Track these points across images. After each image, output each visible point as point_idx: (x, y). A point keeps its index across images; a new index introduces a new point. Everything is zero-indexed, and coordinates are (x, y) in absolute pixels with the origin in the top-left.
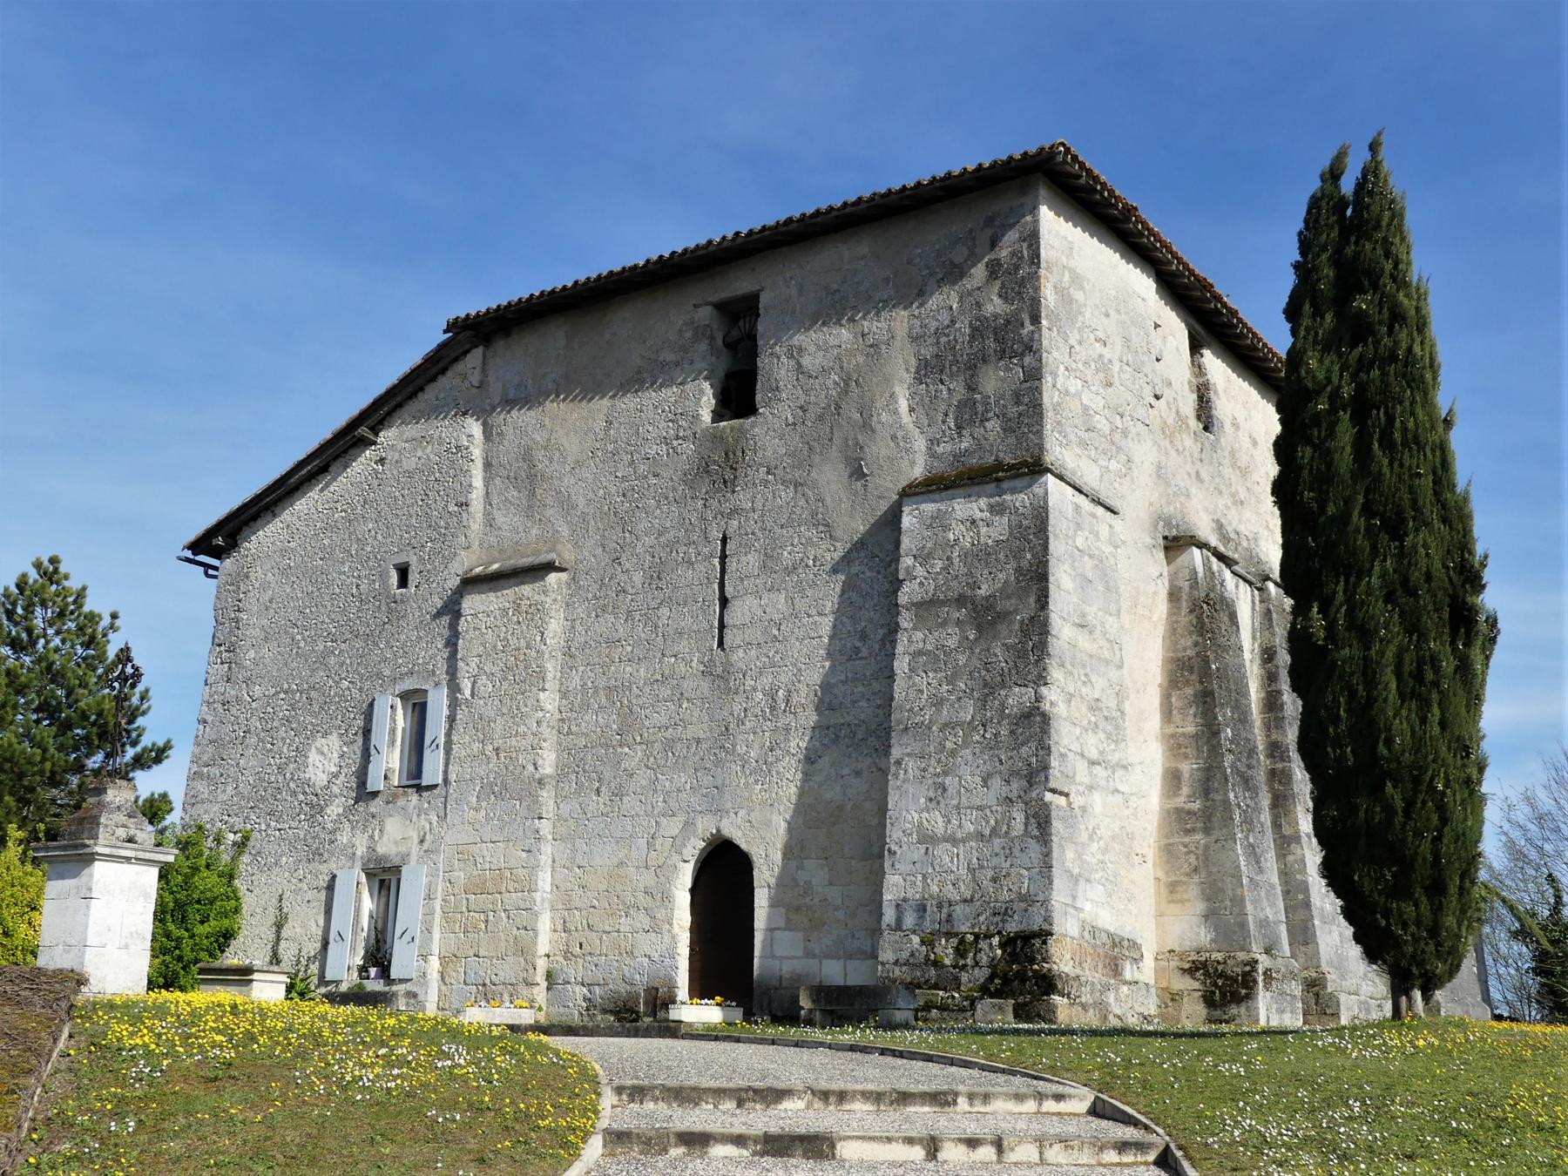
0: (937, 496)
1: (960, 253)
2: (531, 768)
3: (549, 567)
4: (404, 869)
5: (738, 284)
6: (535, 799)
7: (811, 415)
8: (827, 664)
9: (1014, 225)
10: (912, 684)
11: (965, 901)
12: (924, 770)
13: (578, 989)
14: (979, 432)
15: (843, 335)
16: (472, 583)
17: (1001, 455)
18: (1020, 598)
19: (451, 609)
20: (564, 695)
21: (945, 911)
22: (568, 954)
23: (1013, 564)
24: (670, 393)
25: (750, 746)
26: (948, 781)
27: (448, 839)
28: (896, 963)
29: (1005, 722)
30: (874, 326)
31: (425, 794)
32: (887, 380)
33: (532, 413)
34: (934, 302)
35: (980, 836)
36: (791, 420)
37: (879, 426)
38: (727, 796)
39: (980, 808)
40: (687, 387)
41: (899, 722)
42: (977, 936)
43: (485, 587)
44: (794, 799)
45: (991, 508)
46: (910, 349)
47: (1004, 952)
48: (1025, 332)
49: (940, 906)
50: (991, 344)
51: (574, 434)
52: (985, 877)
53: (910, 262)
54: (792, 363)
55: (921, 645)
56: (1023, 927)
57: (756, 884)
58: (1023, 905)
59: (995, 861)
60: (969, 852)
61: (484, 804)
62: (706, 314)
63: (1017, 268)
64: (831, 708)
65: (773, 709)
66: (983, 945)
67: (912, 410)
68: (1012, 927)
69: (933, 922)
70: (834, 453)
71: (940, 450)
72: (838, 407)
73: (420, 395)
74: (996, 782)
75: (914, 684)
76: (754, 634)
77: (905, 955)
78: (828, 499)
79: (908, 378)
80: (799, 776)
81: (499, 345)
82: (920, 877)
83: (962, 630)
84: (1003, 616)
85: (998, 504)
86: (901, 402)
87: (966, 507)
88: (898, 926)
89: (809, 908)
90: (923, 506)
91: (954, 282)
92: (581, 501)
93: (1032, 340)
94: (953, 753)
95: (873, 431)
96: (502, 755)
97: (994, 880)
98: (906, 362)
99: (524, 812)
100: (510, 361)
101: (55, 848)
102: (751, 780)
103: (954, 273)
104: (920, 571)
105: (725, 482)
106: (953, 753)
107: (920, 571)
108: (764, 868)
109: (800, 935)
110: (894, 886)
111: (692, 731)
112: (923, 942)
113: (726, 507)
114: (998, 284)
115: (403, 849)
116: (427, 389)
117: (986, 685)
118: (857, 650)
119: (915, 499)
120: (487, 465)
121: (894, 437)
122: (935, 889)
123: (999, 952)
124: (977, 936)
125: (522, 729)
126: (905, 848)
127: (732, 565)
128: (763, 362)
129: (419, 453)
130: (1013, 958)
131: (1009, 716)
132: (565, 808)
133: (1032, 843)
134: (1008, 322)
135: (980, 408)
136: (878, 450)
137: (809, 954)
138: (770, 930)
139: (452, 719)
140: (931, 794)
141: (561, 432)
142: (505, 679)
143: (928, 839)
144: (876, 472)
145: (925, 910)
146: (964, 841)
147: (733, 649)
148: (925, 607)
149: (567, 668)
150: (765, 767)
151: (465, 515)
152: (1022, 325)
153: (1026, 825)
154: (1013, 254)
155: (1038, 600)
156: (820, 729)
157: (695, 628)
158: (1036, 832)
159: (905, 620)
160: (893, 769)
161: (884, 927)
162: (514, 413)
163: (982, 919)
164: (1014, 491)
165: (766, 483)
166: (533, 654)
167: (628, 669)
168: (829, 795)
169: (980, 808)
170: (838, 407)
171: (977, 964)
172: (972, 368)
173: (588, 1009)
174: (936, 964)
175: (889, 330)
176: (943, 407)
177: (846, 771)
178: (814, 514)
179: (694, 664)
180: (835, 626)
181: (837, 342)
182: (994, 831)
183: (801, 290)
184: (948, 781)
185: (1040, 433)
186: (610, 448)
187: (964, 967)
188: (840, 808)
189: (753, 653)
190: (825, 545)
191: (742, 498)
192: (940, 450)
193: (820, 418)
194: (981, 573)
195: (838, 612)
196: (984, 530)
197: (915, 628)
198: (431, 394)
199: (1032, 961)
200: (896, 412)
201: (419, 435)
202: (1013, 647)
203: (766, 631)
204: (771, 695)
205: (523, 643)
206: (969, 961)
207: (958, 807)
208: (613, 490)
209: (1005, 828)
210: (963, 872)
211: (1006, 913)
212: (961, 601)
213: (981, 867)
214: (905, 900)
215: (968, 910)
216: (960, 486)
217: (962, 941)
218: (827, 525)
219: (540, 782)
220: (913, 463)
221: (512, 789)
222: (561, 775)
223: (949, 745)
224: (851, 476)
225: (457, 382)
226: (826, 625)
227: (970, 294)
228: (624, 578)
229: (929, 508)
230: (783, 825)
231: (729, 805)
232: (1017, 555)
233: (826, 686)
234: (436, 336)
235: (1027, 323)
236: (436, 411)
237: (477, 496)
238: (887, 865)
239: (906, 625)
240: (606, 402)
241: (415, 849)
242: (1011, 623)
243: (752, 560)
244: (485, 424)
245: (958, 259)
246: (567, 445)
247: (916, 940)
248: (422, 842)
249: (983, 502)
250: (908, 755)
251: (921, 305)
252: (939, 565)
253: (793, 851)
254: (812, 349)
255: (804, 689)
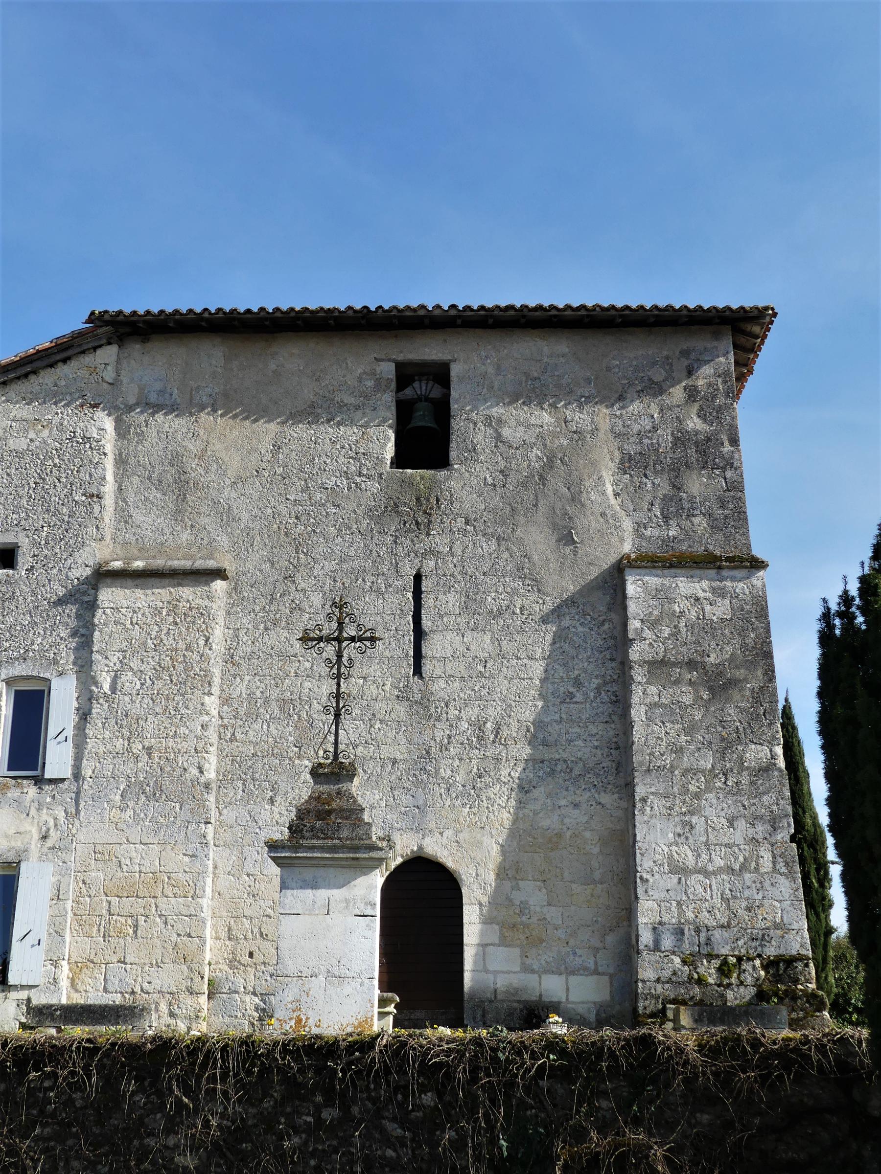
0: (659, 572)
1: (658, 374)
2: (195, 772)
3: (219, 574)
4: (23, 866)
5: (428, 349)
6: (202, 804)
7: (513, 479)
8: (540, 704)
9: (709, 362)
10: (649, 733)
11: (722, 926)
12: (670, 809)
13: (248, 998)
14: (686, 524)
15: (545, 418)
16: (103, 576)
17: (711, 548)
18: (748, 669)
19: (83, 598)
20: (225, 701)
21: (703, 935)
22: (233, 963)
23: (736, 641)
24: (350, 433)
25: (454, 769)
26: (694, 820)
27: (81, 837)
28: (658, 980)
29: (745, 773)
30: (580, 418)
31: (46, 787)
32: (594, 464)
33: (182, 421)
34: (635, 407)
35: (730, 870)
36: (490, 480)
37: (588, 503)
38: (430, 816)
39: (727, 846)
40: (371, 431)
41: (641, 764)
42: (740, 959)
43: (129, 582)
44: (507, 824)
45: (714, 590)
46: (614, 444)
47: (767, 973)
48: (725, 450)
49: (698, 930)
50: (692, 452)
51: (229, 448)
52: (740, 907)
53: (609, 369)
54: (490, 431)
55: (656, 699)
56: (782, 951)
57: (465, 900)
58: (779, 932)
59: (747, 893)
60: (722, 883)
61: (131, 804)
62: (388, 370)
63: (714, 397)
64: (545, 744)
65: (480, 739)
66: (745, 966)
67: (616, 495)
68: (771, 951)
69: (691, 944)
70: (540, 516)
71: (648, 532)
72: (542, 478)
73: (32, 378)
74: (741, 824)
75: (653, 732)
76: (458, 668)
77: (667, 973)
78: (535, 557)
79: (613, 466)
80: (512, 802)
81: (135, 348)
82: (674, 904)
83: (696, 691)
84: (733, 683)
85: (719, 588)
86: (606, 484)
87: (688, 587)
88: (656, 947)
89: (526, 926)
90: (646, 578)
91: (654, 396)
92: (245, 516)
93: (732, 458)
94: (697, 796)
95: (583, 505)
96: (156, 755)
97: (749, 909)
98: (611, 453)
99: (185, 815)
100: (148, 366)
101: (322, 849)
102: (458, 803)
103: (655, 389)
104: (647, 634)
105: (417, 523)
106: (697, 796)
107: (647, 634)
108: (475, 887)
109: (517, 951)
110: (647, 913)
111: (386, 752)
112: (684, 962)
113: (420, 547)
114: (695, 407)
115: (18, 844)
116: (42, 373)
117: (723, 739)
118: (571, 695)
119: (639, 571)
120: (121, 461)
121: (603, 514)
122: (690, 915)
123: (762, 973)
124: (740, 959)
125: (182, 730)
126: (657, 876)
127: (428, 602)
128: (457, 424)
129: (32, 435)
130: (777, 978)
131: (748, 768)
132: (229, 815)
133: (782, 880)
134: (708, 439)
135: (686, 505)
136: (588, 523)
137: (526, 969)
138: (483, 946)
139: (84, 716)
140: (679, 830)
141: (219, 446)
142: (159, 678)
143: (678, 870)
144: (587, 541)
145: (683, 934)
146: (714, 873)
147: (432, 679)
148: (658, 667)
149: (230, 677)
150: (474, 790)
151: (97, 508)
152: (722, 444)
153: (774, 863)
154: (710, 385)
155: (765, 674)
156: (533, 762)
157: (387, 654)
158: (784, 870)
159: (639, 675)
160: (639, 805)
161: (641, 947)
162: (159, 417)
163: (741, 943)
164: (733, 579)
165: (465, 533)
166: (195, 657)
167: (307, 684)
168: (546, 823)
169: (727, 846)
170: (542, 478)
171: (742, 983)
172: (676, 472)
173: (260, 1019)
174: (700, 981)
175: (592, 422)
176: (648, 497)
177: (563, 802)
178: (520, 568)
179: (387, 688)
180: (546, 671)
181: (538, 422)
182: (744, 867)
183: (498, 369)
184: (694, 820)
185: (746, 534)
186: (280, 470)
187: (729, 985)
188: (559, 835)
189: (457, 684)
190: (533, 597)
191: (440, 542)
192: (648, 532)
193: (524, 485)
194: (708, 643)
195: (549, 658)
196: (708, 608)
197: (649, 683)
198: (47, 378)
199: (796, 981)
200: (604, 493)
201: (31, 417)
202: (747, 710)
203: (470, 667)
204: (479, 726)
205: (181, 645)
206: (734, 980)
207: (706, 844)
208: (284, 511)
209: (753, 865)
210: (717, 901)
211: (763, 939)
212: (691, 665)
213: (735, 897)
214: (661, 923)
215: (726, 934)
216: (684, 567)
217: (725, 962)
218: (535, 580)
219: (207, 786)
220: (622, 540)
221: (163, 790)
222: (224, 779)
223: (692, 788)
224: (559, 540)
225: (84, 373)
226: (537, 669)
227: (670, 408)
228: (299, 596)
229: (653, 581)
230: (496, 848)
231: (433, 825)
232: (742, 632)
233: (539, 724)
234: (77, 323)
235: (726, 443)
236: (55, 396)
237: (109, 489)
238: (640, 891)
239: (639, 679)
240: (273, 427)
241: (35, 845)
242: (741, 690)
243: (452, 600)
244: (118, 422)
245: (658, 378)
246: (226, 459)
247: (677, 960)
248: (45, 838)
249: (705, 584)
250: (653, 793)
251: (622, 408)
252: (667, 632)
253: (507, 872)
254: (513, 423)
255: (515, 725)
